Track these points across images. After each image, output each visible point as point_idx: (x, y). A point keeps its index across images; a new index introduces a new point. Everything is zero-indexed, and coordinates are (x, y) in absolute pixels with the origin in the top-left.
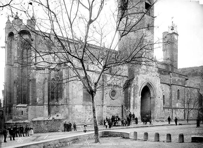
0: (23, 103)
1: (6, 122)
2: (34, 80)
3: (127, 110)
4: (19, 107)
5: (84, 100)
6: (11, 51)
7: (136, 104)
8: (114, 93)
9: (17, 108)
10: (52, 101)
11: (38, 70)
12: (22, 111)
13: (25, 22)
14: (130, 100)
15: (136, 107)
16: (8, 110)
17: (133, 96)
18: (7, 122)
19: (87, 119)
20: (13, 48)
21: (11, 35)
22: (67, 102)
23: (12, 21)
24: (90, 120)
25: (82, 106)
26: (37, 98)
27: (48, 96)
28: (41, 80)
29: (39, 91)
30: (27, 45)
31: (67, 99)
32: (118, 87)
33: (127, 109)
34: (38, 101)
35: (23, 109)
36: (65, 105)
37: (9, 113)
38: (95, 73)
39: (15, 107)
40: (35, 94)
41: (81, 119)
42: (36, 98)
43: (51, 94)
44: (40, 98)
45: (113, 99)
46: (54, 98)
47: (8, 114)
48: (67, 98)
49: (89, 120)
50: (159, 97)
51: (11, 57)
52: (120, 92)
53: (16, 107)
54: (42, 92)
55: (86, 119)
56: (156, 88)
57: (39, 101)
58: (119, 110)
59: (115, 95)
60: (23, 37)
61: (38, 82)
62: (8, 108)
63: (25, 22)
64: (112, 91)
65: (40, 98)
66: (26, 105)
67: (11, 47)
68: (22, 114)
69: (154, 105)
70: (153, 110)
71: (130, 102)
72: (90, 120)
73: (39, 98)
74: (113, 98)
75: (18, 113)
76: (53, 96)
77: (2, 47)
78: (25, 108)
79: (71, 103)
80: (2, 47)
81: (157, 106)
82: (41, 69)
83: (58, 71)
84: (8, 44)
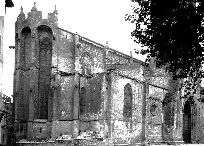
0: (40, 119)
1: (18, 141)
2: (60, 88)
3: (168, 129)
4: (36, 122)
5: (124, 115)
6: (25, 51)
7: (179, 122)
8: (153, 108)
9: (34, 124)
10: (81, 116)
11: (65, 75)
12: (41, 128)
13: (45, 17)
14: (173, 117)
15: (179, 125)
16: (20, 126)
17: (177, 113)
18: (20, 142)
19: (127, 139)
20: (27, 49)
21: (26, 31)
22: (107, 116)
23: (28, 14)
24: (131, 140)
25: (122, 122)
26: (63, 111)
27: (78, 108)
28: (68, 89)
29: (65, 102)
30: (46, 47)
31: (107, 112)
32: (158, 101)
33: (169, 127)
34: (63, 115)
35: (41, 126)
36: (105, 120)
37: (21, 131)
38: (136, 83)
39: (32, 123)
40: (60, 105)
41: (121, 138)
42: (61, 112)
43: (81, 107)
44: (67, 112)
45: (153, 115)
46: (83, 112)
47: (20, 131)
48: (107, 112)
49: (129, 140)
50: (199, 115)
51: (24, 59)
52: (160, 106)
53: (33, 123)
54: (69, 104)
55: (126, 138)
56: (197, 104)
57: (65, 115)
58: (158, 129)
59: (155, 110)
60: (36, 36)
61: (64, 90)
62: (20, 125)
63: (45, 17)
64: (152, 105)
65: (67, 112)
66: (45, 121)
67: (24, 46)
68: (41, 132)
69: (195, 123)
70: (193, 130)
71: (173, 119)
72: (131, 140)
73: (65, 112)
74: (153, 113)
75: (35, 130)
76: (82, 109)
77: (11, 47)
78: (44, 124)
79: (112, 118)
80: (11, 47)
81: (197, 125)
82: (68, 75)
83: (89, 78)
84: (21, 42)
